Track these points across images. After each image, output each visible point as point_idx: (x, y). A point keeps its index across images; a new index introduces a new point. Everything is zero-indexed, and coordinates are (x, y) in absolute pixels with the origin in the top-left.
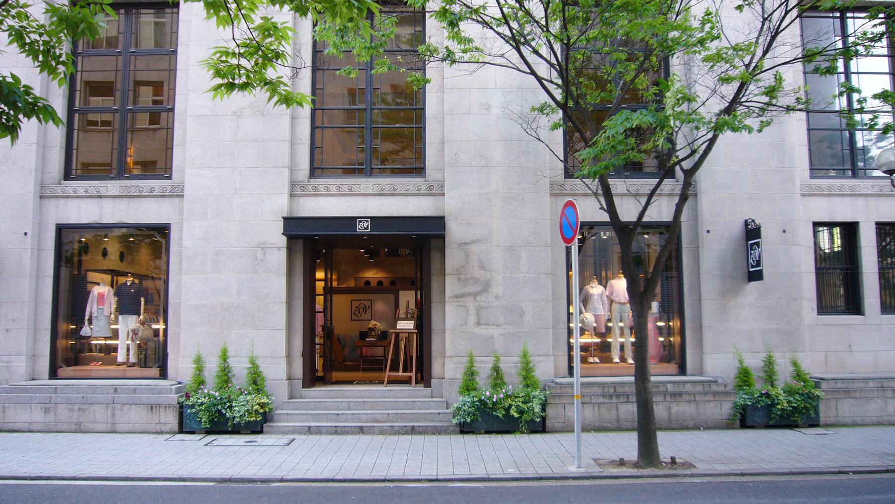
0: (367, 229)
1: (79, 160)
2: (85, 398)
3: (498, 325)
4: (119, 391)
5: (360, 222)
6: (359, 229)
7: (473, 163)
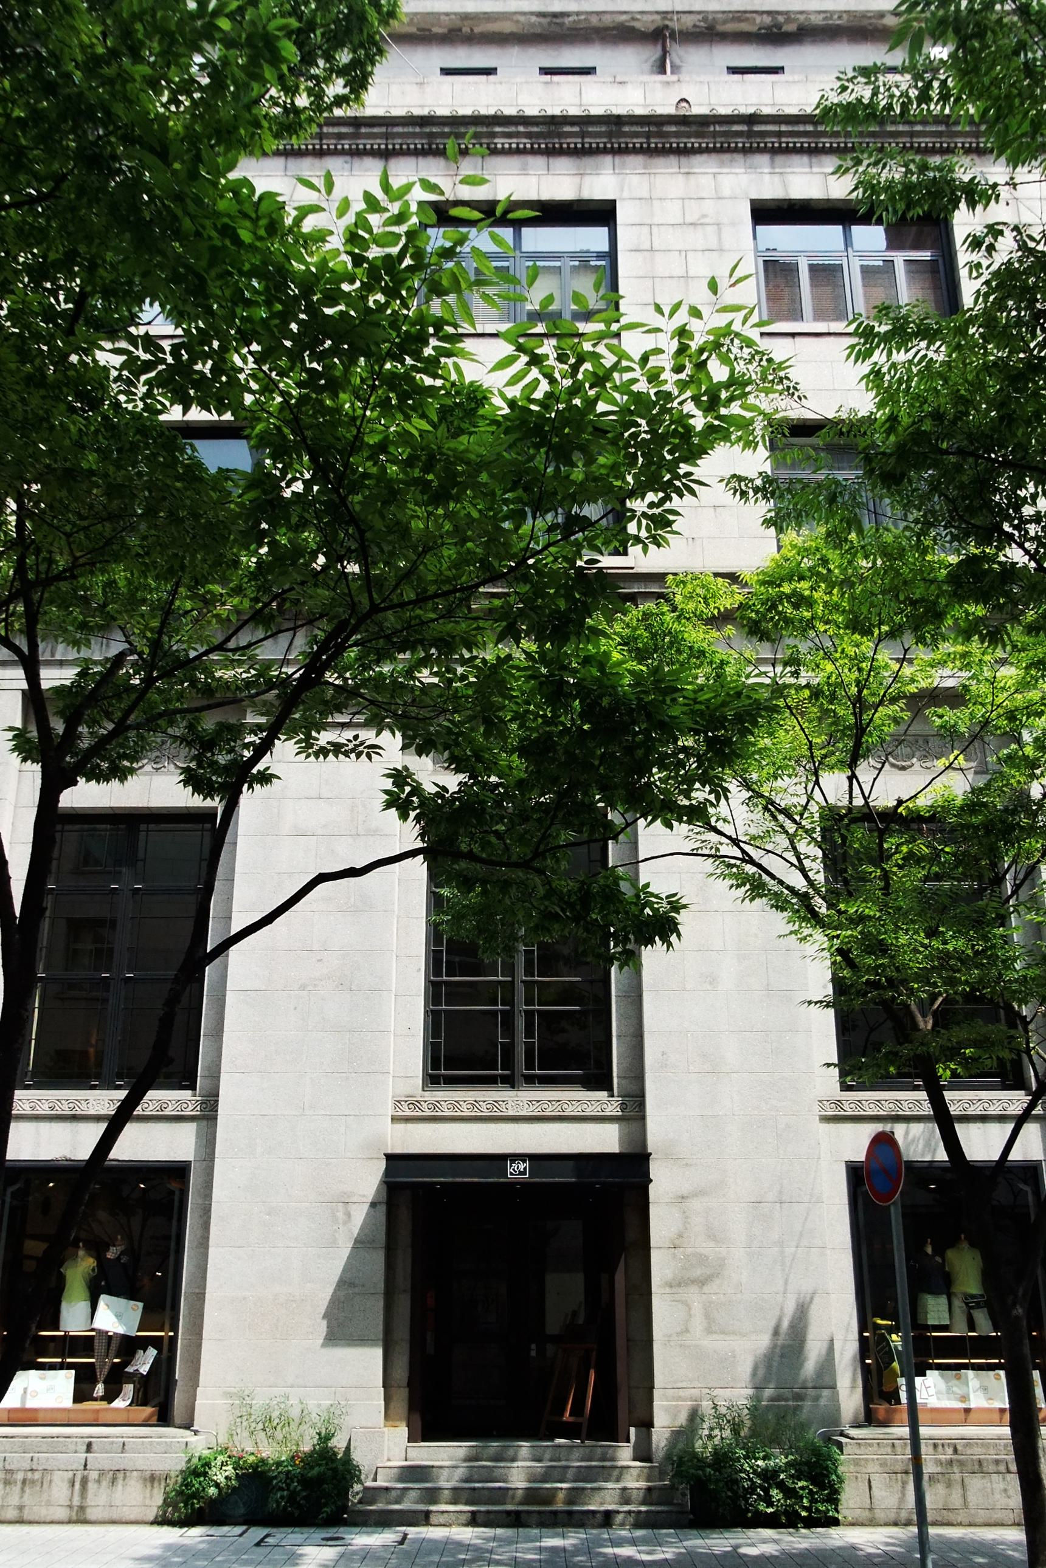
0: (524, 1173)
1: (171, 333)
2: (35, 1459)
3: (743, 1335)
4: (95, 1447)
5: (513, 1161)
6: (511, 1174)
7: (692, 1068)
